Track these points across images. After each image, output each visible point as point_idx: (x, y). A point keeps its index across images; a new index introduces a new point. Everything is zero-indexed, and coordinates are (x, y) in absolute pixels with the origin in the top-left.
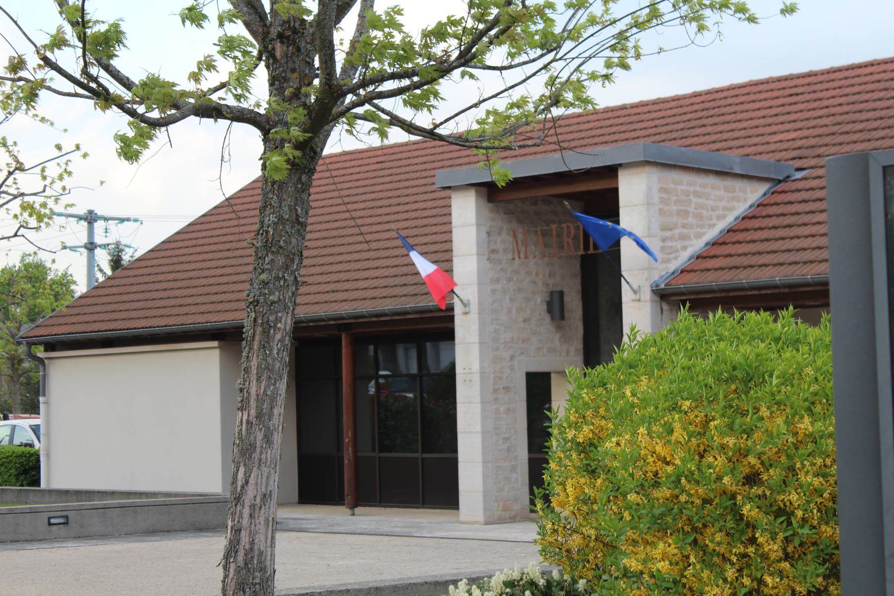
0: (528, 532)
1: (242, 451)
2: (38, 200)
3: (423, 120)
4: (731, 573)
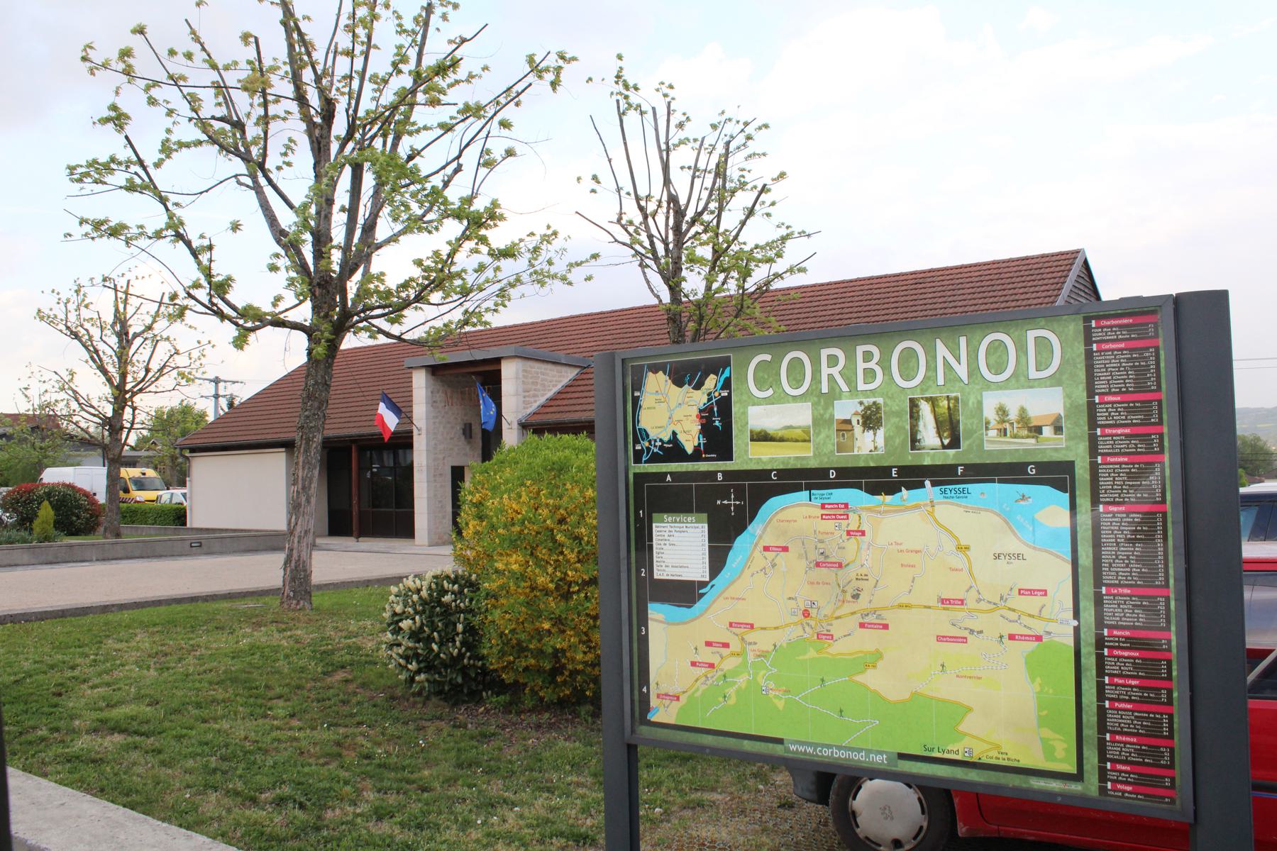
0: (448, 550)
1: (295, 507)
2: (187, 370)
3: (396, 330)
4: (550, 570)
